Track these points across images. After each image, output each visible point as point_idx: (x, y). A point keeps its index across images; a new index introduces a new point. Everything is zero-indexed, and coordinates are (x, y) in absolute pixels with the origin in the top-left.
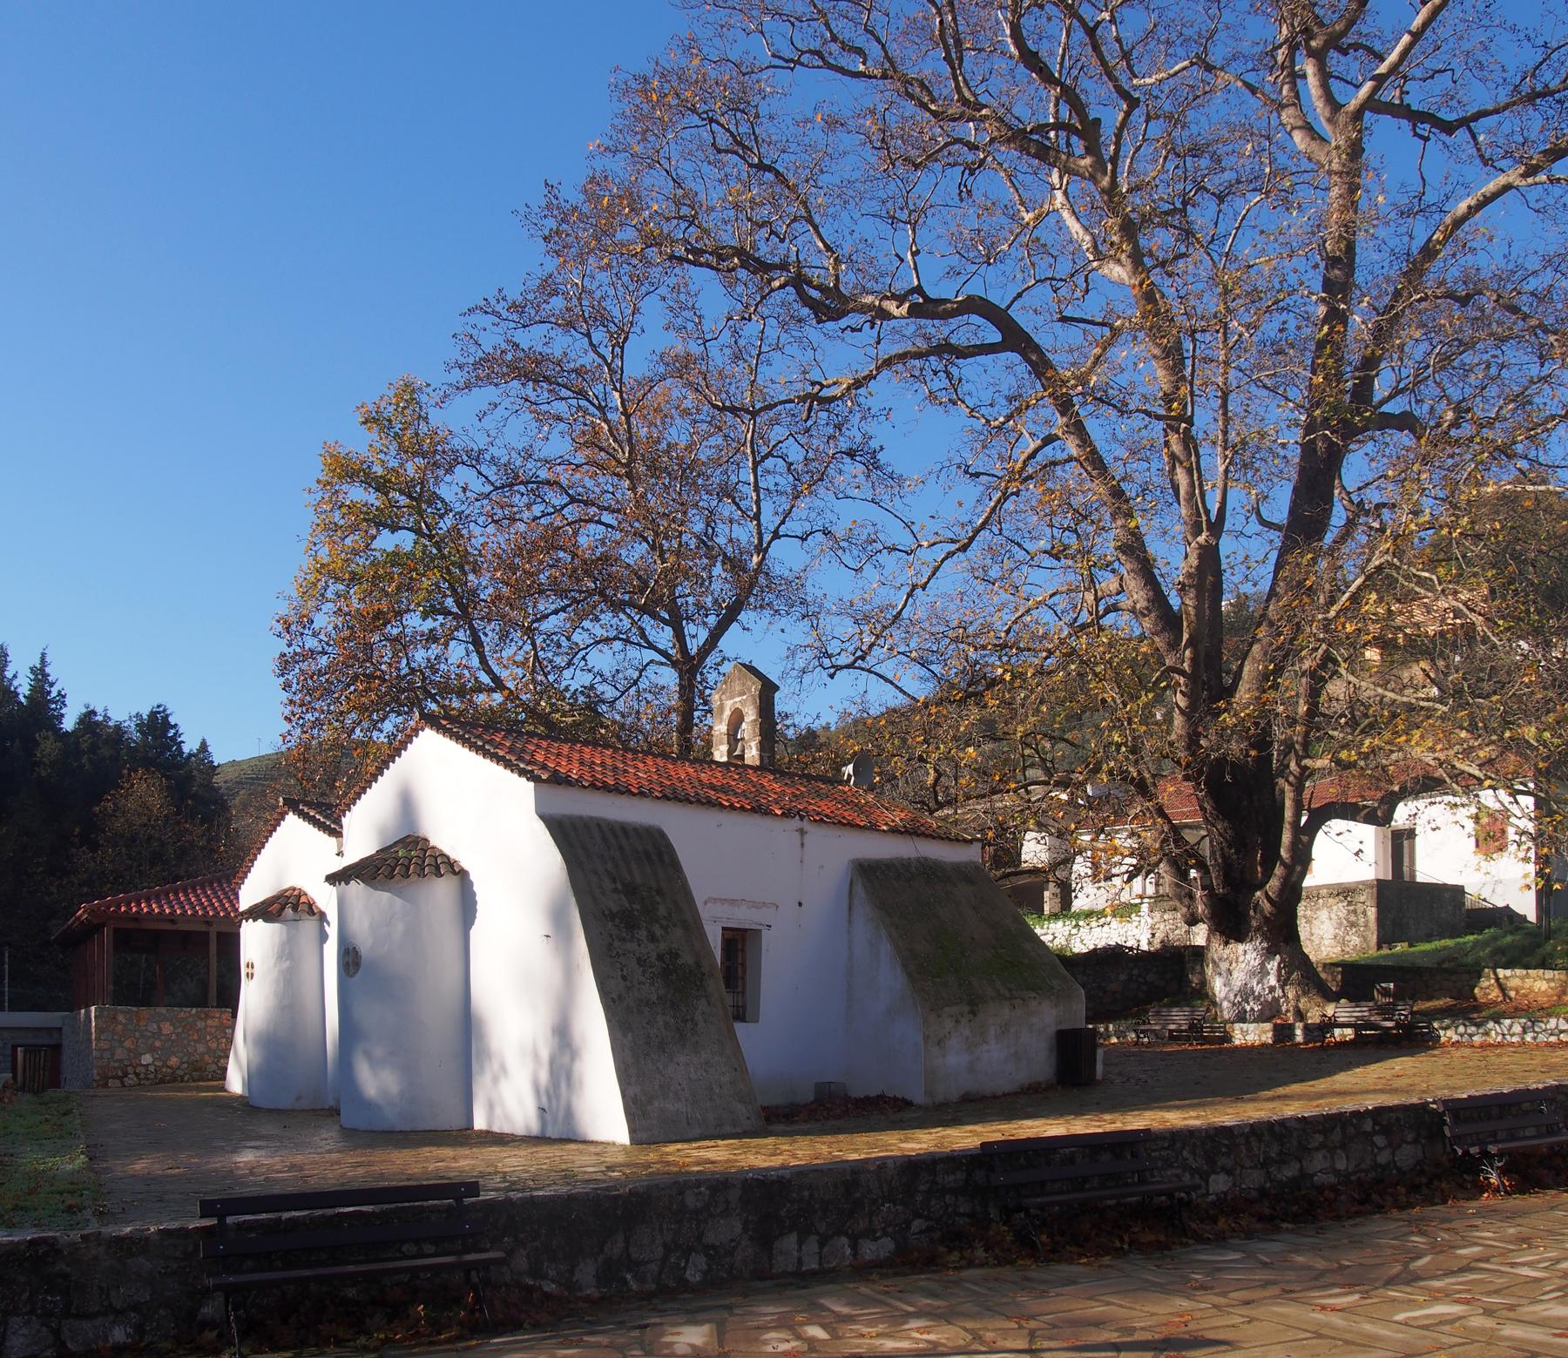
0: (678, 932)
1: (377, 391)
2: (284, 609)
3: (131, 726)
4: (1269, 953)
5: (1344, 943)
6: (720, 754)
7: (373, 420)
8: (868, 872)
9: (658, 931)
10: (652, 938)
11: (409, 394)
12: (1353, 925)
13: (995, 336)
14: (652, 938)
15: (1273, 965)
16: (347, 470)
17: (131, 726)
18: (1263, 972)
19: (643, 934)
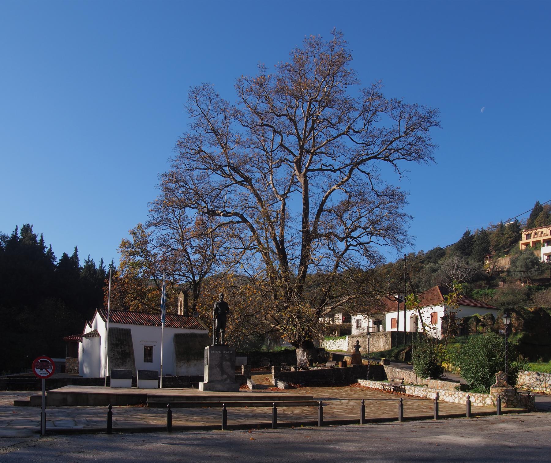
0: (127, 347)
1: (133, 227)
2: (168, 169)
3: (58, 256)
4: (304, 351)
5: (385, 347)
6: (179, 314)
7: (133, 233)
8: (177, 336)
9: (123, 347)
10: (121, 348)
11: (140, 227)
12: (387, 343)
13: (240, 220)
14: (121, 348)
15: (305, 353)
16: (125, 244)
17: (58, 256)
18: (304, 355)
19: (119, 347)
